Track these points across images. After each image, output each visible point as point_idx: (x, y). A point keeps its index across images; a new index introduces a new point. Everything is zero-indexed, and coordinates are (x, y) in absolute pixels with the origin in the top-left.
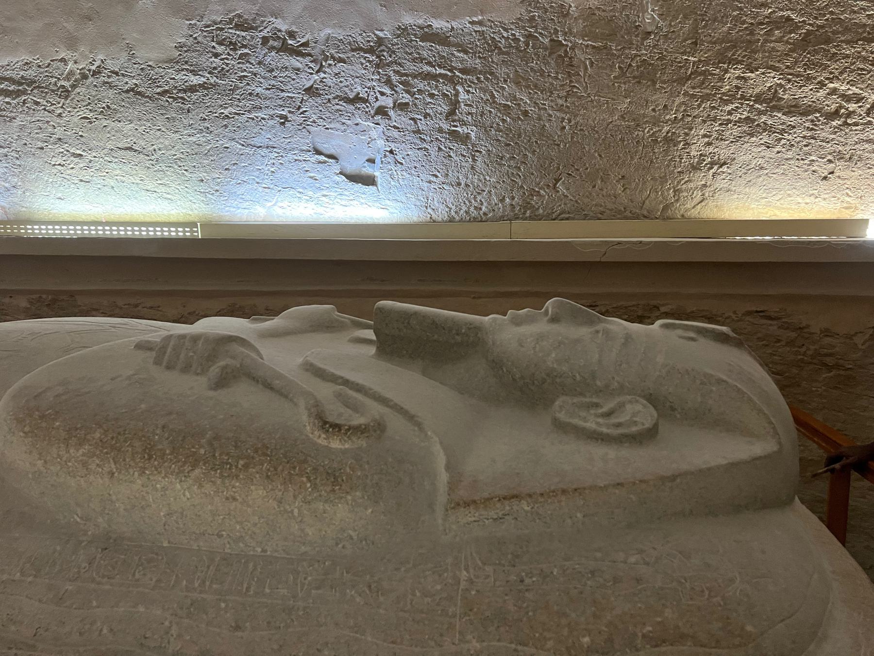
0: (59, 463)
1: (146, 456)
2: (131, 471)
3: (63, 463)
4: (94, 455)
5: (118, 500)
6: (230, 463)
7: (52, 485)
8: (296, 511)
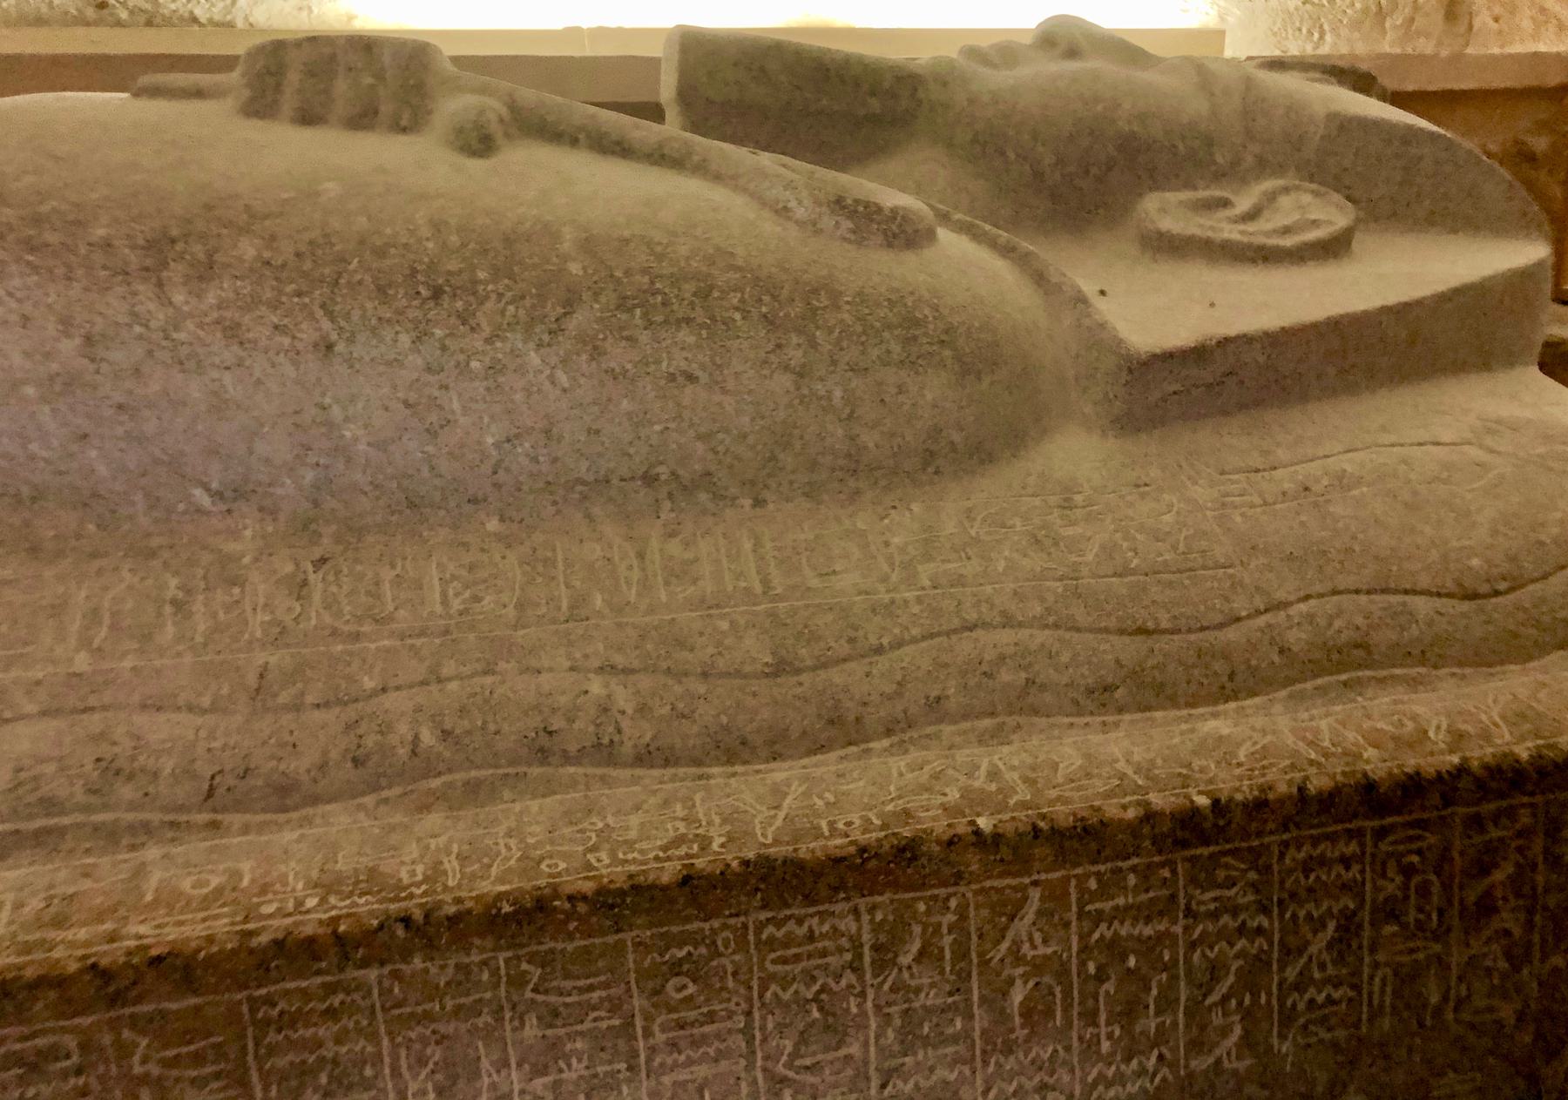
0: (140, 337)
1: (424, 292)
2: (388, 334)
3: (157, 336)
4: (255, 302)
5: (347, 419)
6: (658, 292)
7: (120, 407)
8: (838, 393)
